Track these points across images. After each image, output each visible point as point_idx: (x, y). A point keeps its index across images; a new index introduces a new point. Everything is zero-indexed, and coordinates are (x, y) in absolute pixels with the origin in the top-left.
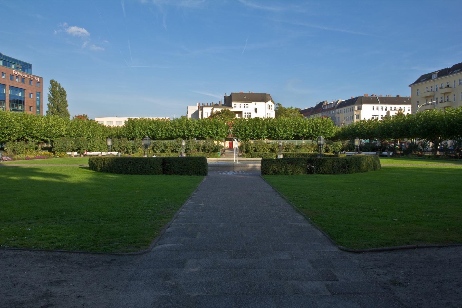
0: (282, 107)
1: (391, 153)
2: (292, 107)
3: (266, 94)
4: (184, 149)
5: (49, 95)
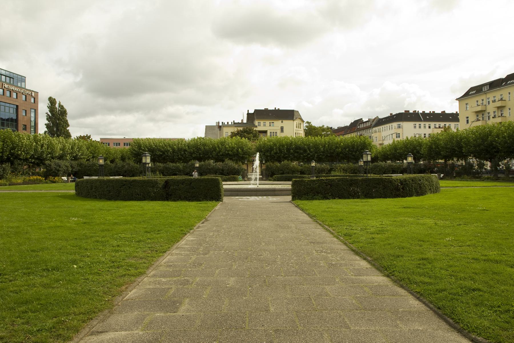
0: (311, 126)
1: (442, 175)
2: (323, 126)
3: (293, 111)
4: (112, 102)
5: (47, 113)
